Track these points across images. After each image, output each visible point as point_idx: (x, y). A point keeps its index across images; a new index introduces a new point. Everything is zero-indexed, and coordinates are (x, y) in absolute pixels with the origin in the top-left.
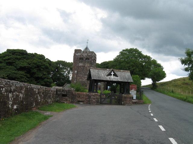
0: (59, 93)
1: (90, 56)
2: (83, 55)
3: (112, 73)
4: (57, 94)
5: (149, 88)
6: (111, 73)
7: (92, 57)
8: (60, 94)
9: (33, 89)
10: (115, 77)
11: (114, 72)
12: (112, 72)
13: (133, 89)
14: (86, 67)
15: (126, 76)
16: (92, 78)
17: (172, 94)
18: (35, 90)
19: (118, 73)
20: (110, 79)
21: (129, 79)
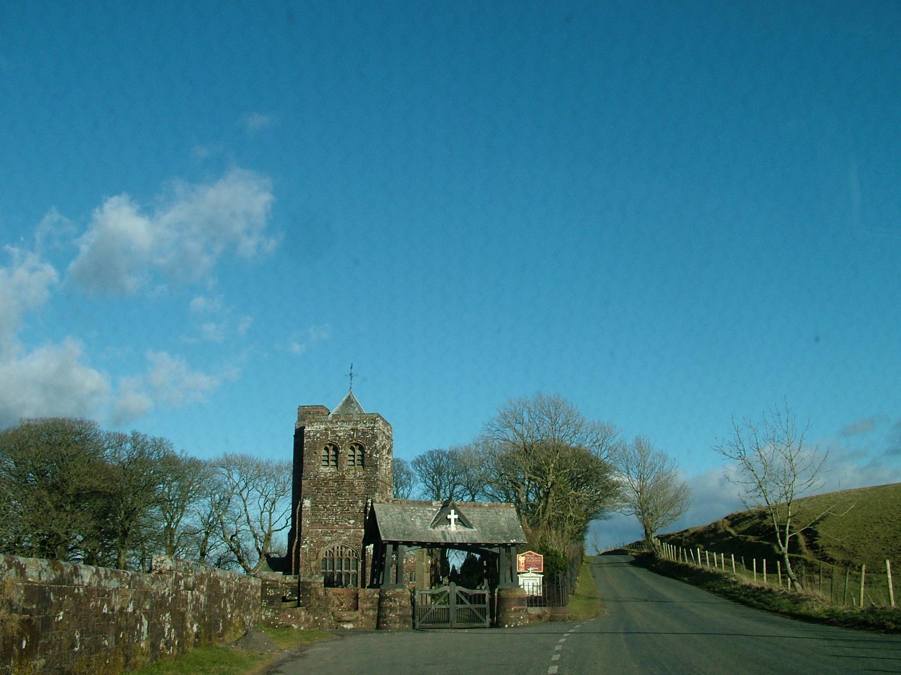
0: (271, 592)
1: (364, 433)
2: (334, 432)
3: (453, 516)
4: (264, 596)
5: (758, 466)
6: (449, 517)
7: (375, 437)
8: (277, 596)
9: (219, 582)
10: (462, 529)
11: (457, 512)
12: (453, 511)
13: (530, 569)
14: (351, 484)
15: (503, 522)
16: (383, 538)
17: (448, 625)
18: (221, 583)
19: (473, 515)
20: (445, 537)
21: (513, 532)
